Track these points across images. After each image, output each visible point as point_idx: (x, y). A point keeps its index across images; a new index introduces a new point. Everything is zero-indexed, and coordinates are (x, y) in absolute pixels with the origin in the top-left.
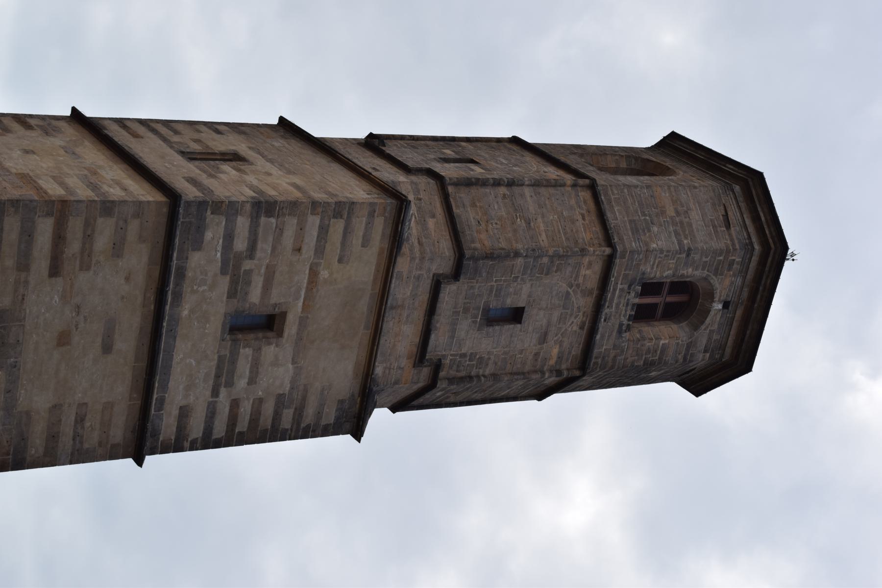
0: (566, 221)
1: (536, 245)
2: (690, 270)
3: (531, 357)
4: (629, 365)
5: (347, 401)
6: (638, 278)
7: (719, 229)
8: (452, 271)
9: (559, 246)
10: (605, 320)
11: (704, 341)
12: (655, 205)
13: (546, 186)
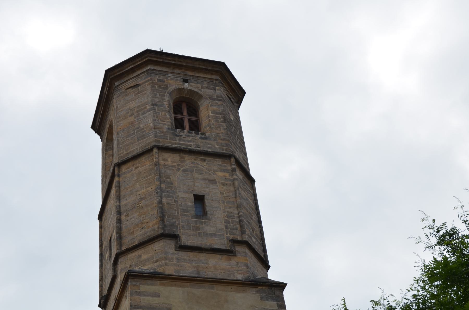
0: (139, 177)
1: (154, 192)
2: (165, 103)
3: (225, 188)
4: (226, 131)
5: (261, 295)
6: (172, 131)
7: (140, 90)
8: (173, 240)
9: (154, 179)
10: (199, 148)
11: (208, 91)
12: (128, 128)
13: (120, 192)
